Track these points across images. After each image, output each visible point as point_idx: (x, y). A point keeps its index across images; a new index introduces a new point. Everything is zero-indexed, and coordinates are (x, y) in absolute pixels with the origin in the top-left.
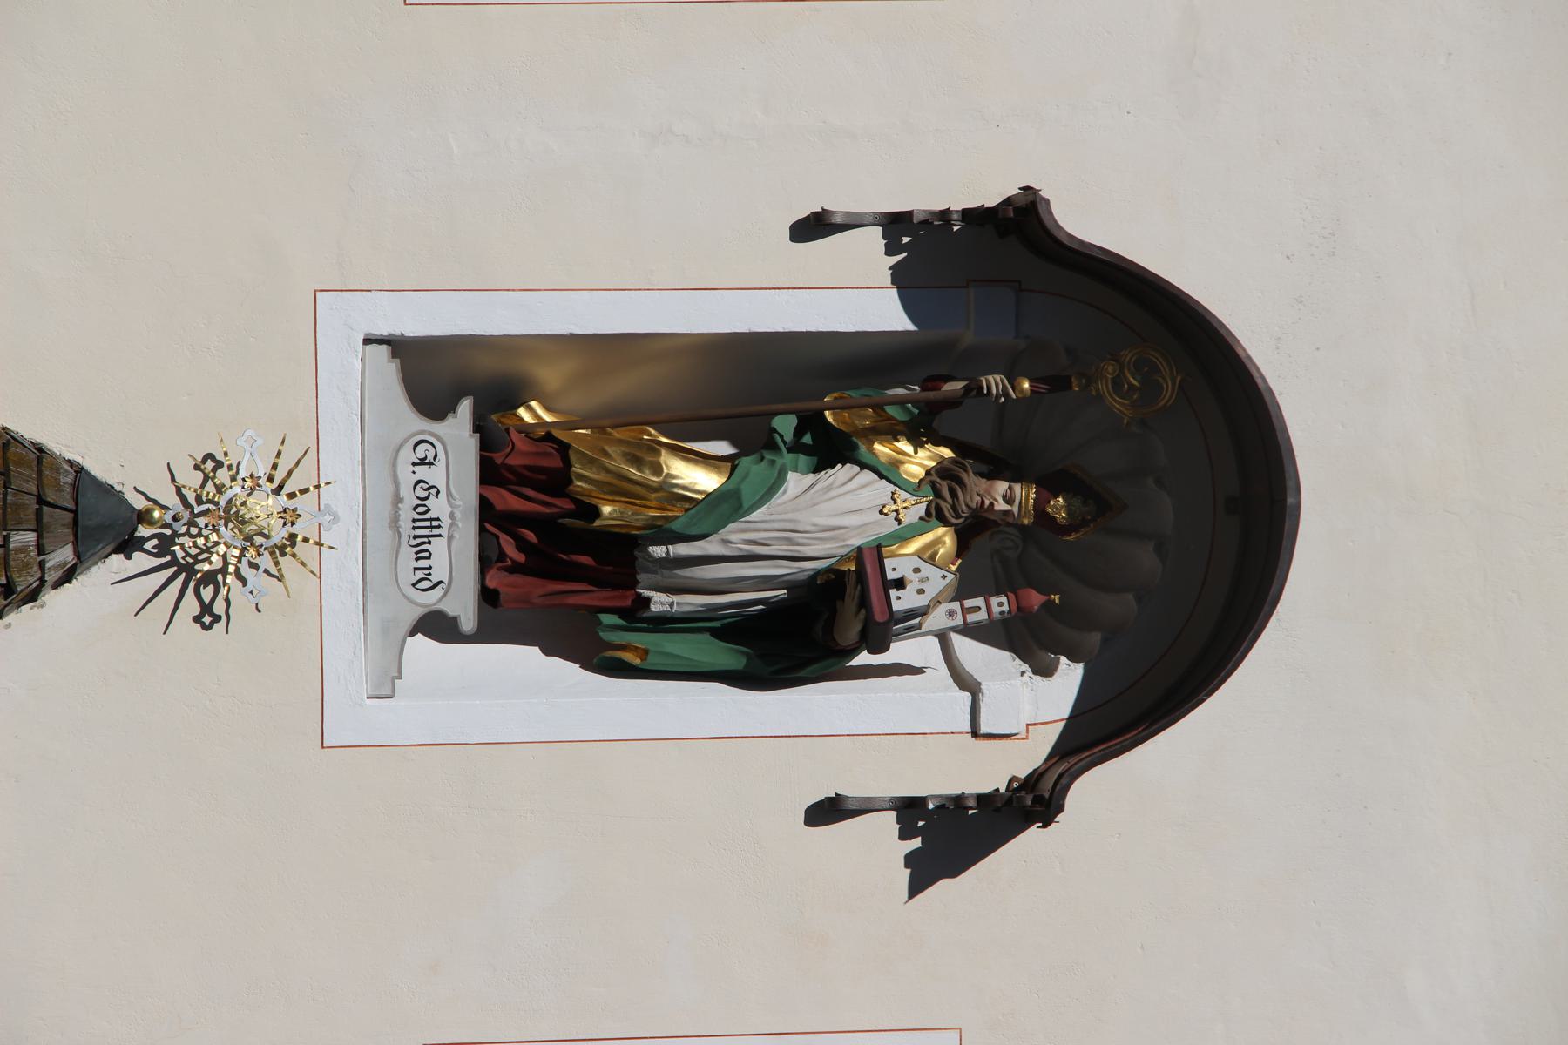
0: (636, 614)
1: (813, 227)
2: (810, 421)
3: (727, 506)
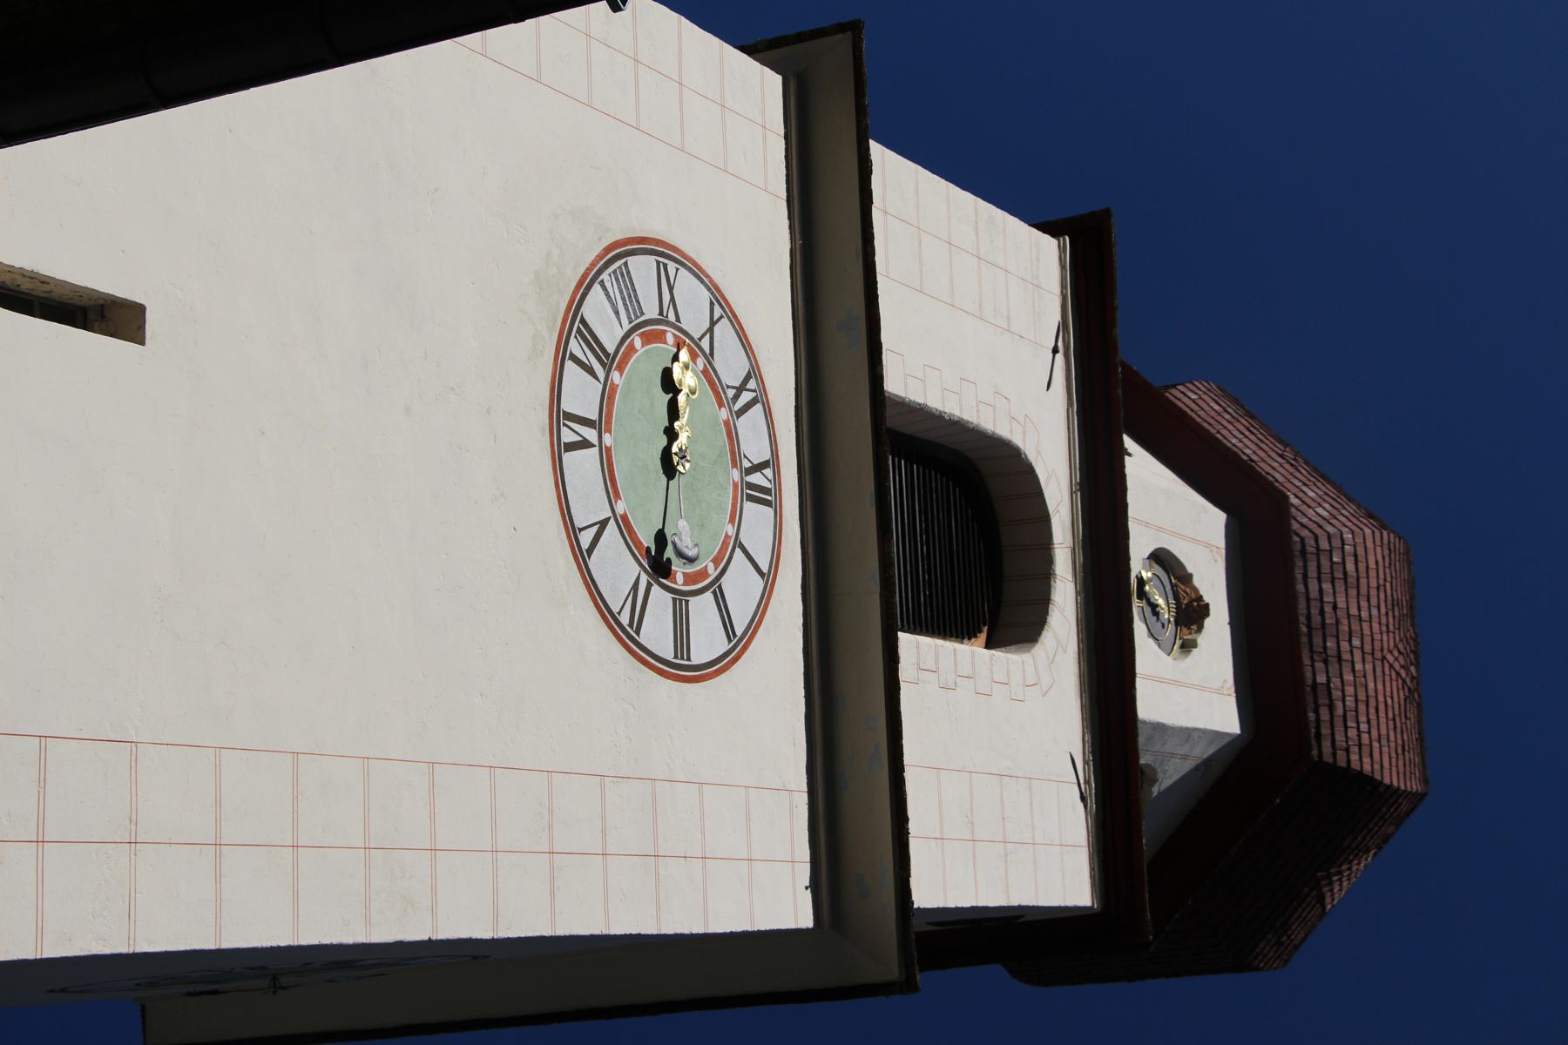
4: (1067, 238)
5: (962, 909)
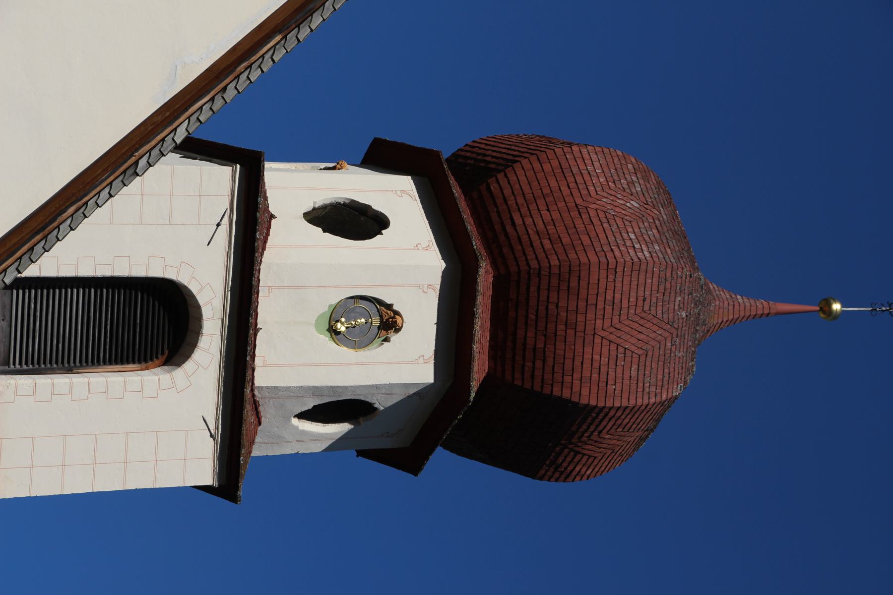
4: (238, 166)
5: (429, 223)
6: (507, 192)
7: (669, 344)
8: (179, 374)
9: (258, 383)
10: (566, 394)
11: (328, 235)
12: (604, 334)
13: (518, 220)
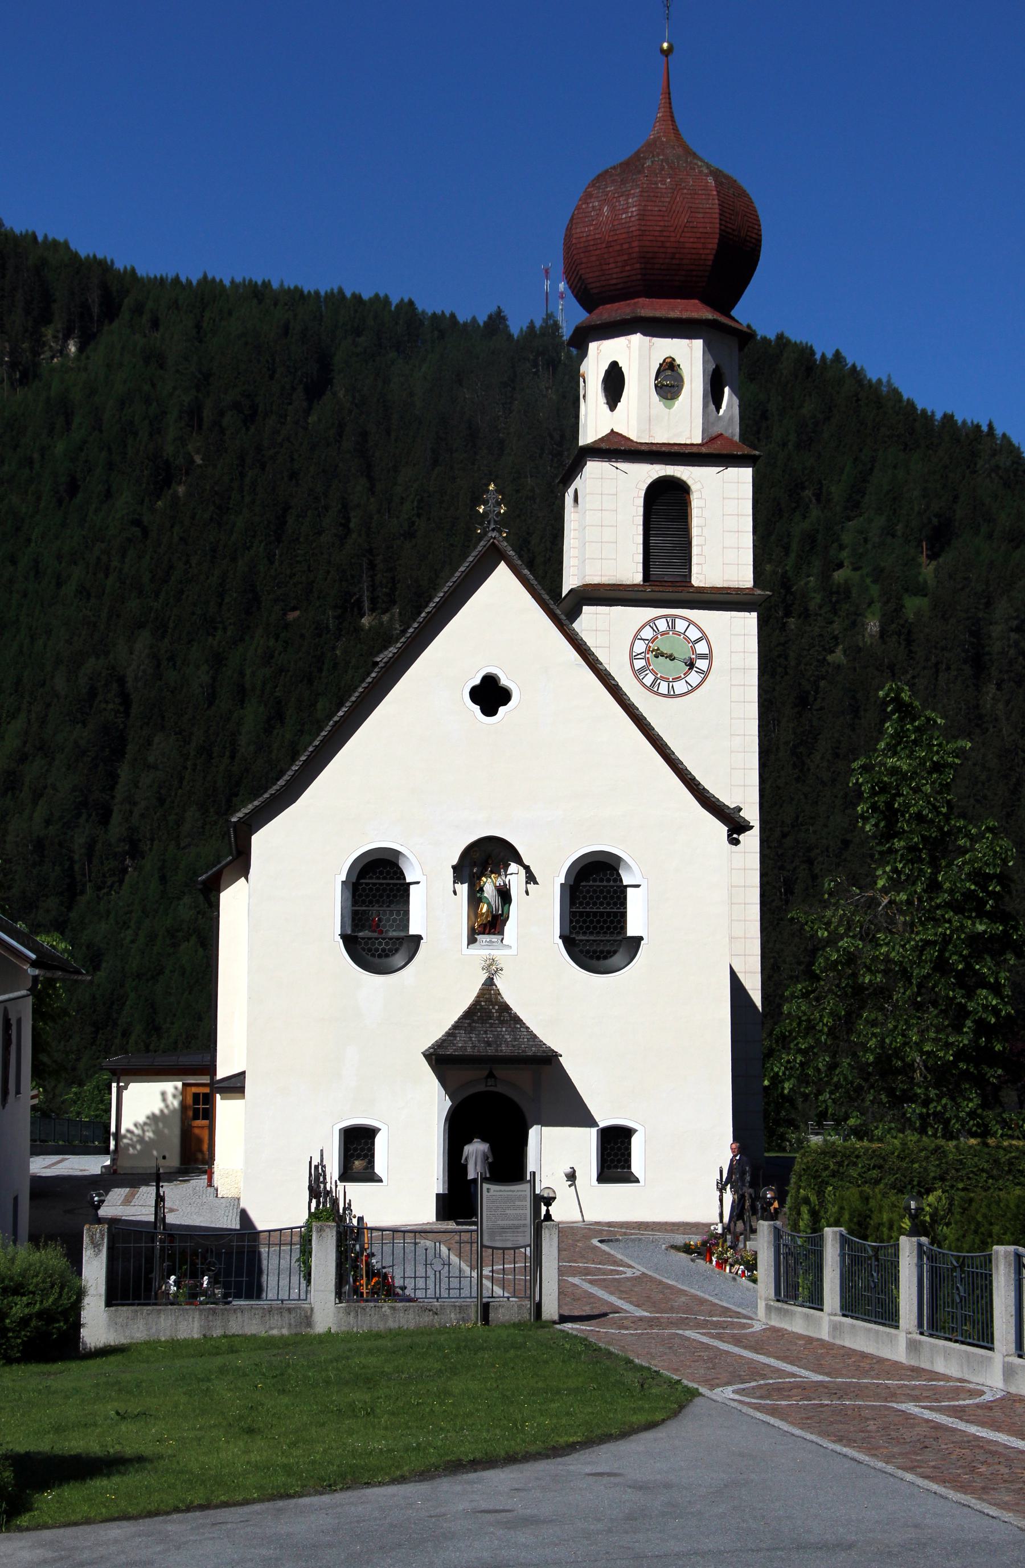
0: (502, 915)
1: (455, 893)
2: (478, 892)
3: (489, 904)
6: (598, 284)
7: (685, 191)
8: (694, 487)
9: (698, 440)
10: (711, 257)
11: (622, 400)
12: (678, 236)
13: (614, 281)
